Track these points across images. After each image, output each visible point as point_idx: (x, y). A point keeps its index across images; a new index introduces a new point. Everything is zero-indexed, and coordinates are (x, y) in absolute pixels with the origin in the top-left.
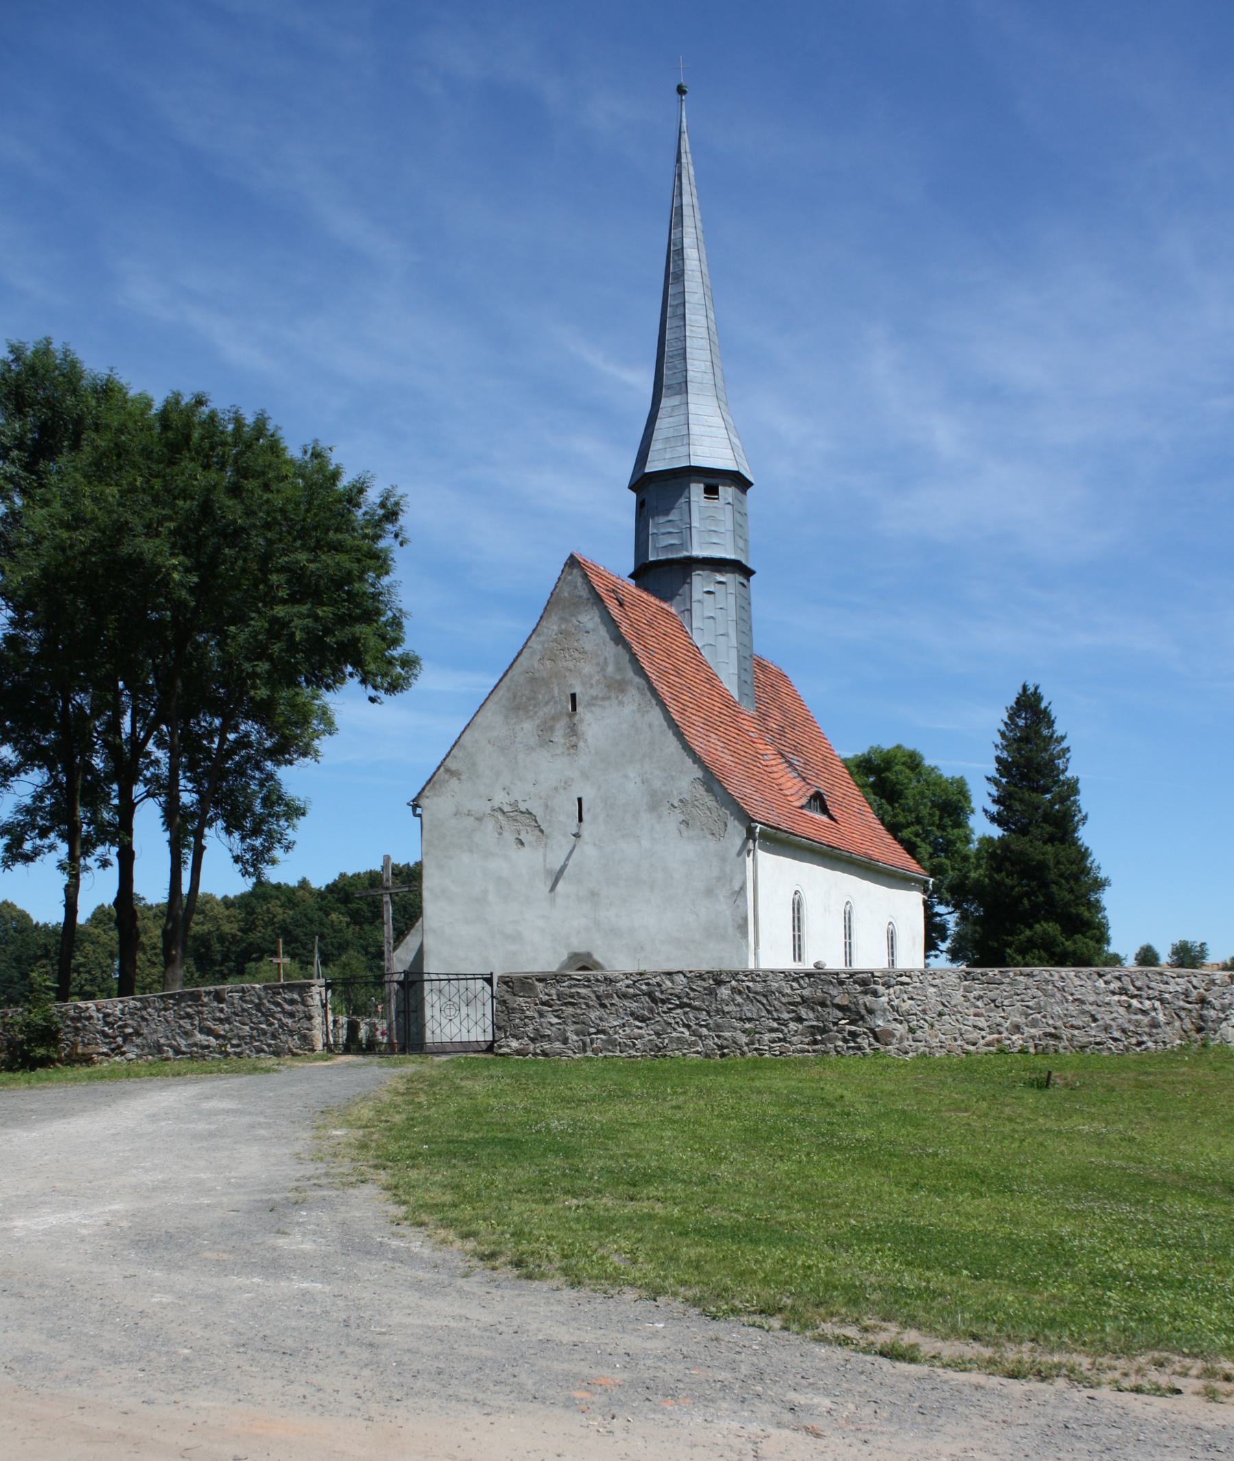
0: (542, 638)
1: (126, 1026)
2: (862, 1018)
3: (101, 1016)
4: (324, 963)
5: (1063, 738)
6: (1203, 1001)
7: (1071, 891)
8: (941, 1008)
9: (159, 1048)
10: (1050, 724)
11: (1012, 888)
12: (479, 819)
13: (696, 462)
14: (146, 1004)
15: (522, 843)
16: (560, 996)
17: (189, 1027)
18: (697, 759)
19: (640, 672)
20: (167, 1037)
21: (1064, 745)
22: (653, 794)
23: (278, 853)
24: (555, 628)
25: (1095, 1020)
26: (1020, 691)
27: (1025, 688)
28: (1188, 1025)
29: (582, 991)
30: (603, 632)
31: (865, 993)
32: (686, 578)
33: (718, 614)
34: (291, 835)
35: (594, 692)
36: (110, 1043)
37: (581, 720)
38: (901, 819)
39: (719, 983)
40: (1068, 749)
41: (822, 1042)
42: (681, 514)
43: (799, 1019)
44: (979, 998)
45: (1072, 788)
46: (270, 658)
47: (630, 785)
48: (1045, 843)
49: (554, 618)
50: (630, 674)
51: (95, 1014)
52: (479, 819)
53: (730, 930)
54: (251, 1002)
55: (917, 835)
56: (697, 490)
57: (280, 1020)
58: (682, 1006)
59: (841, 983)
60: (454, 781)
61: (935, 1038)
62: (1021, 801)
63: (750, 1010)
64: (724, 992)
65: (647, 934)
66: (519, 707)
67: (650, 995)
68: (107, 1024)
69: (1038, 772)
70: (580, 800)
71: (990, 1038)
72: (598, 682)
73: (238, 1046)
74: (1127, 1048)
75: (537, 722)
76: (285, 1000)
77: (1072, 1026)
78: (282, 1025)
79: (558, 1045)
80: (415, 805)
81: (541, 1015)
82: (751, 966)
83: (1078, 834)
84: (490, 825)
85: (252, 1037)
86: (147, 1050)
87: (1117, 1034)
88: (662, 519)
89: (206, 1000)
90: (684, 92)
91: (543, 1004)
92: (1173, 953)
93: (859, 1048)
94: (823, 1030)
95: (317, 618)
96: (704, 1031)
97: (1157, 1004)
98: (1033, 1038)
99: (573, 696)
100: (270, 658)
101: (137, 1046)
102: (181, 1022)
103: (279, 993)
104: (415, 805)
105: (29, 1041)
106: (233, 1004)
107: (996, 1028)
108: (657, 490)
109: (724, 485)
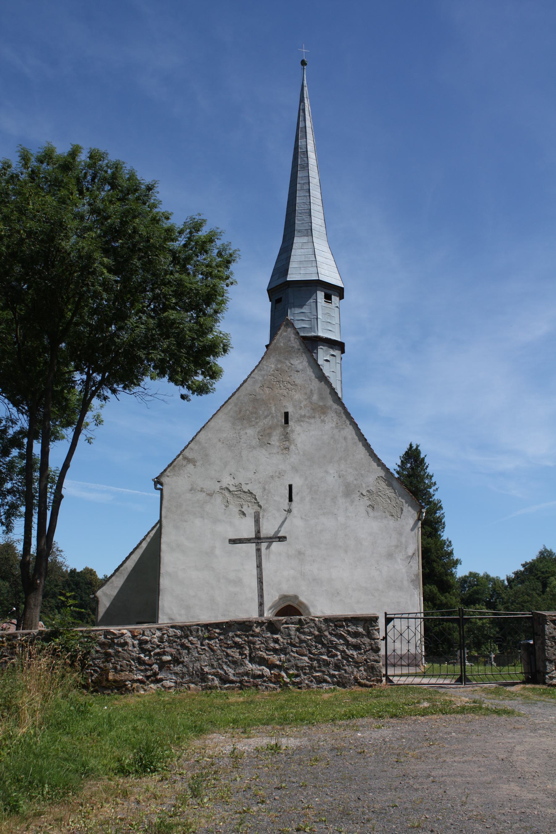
0: (263, 372)
1: (164, 653)
3: (136, 642)
4: (44, 597)
12: (210, 495)
15: (244, 514)
17: (237, 656)
20: (212, 666)
22: (347, 486)
24: (273, 366)
26: (408, 447)
27: (411, 446)
36: (146, 670)
37: (293, 431)
42: (311, 309)
47: (331, 478)
49: (272, 360)
50: (330, 402)
51: (129, 641)
53: (406, 583)
54: (311, 634)
56: (320, 295)
57: (344, 651)
60: (190, 467)
68: (143, 650)
70: (290, 487)
72: (305, 406)
73: (297, 676)
76: (349, 633)
78: (346, 657)
80: (158, 482)
85: (311, 667)
86: (187, 678)
88: (297, 311)
89: (257, 630)
90: (306, 64)
99: (286, 415)
101: (176, 674)
102: (229, 651)
103: (342, 626)
104: (158, 482)
106: (289, 635)
109: (334, 295)
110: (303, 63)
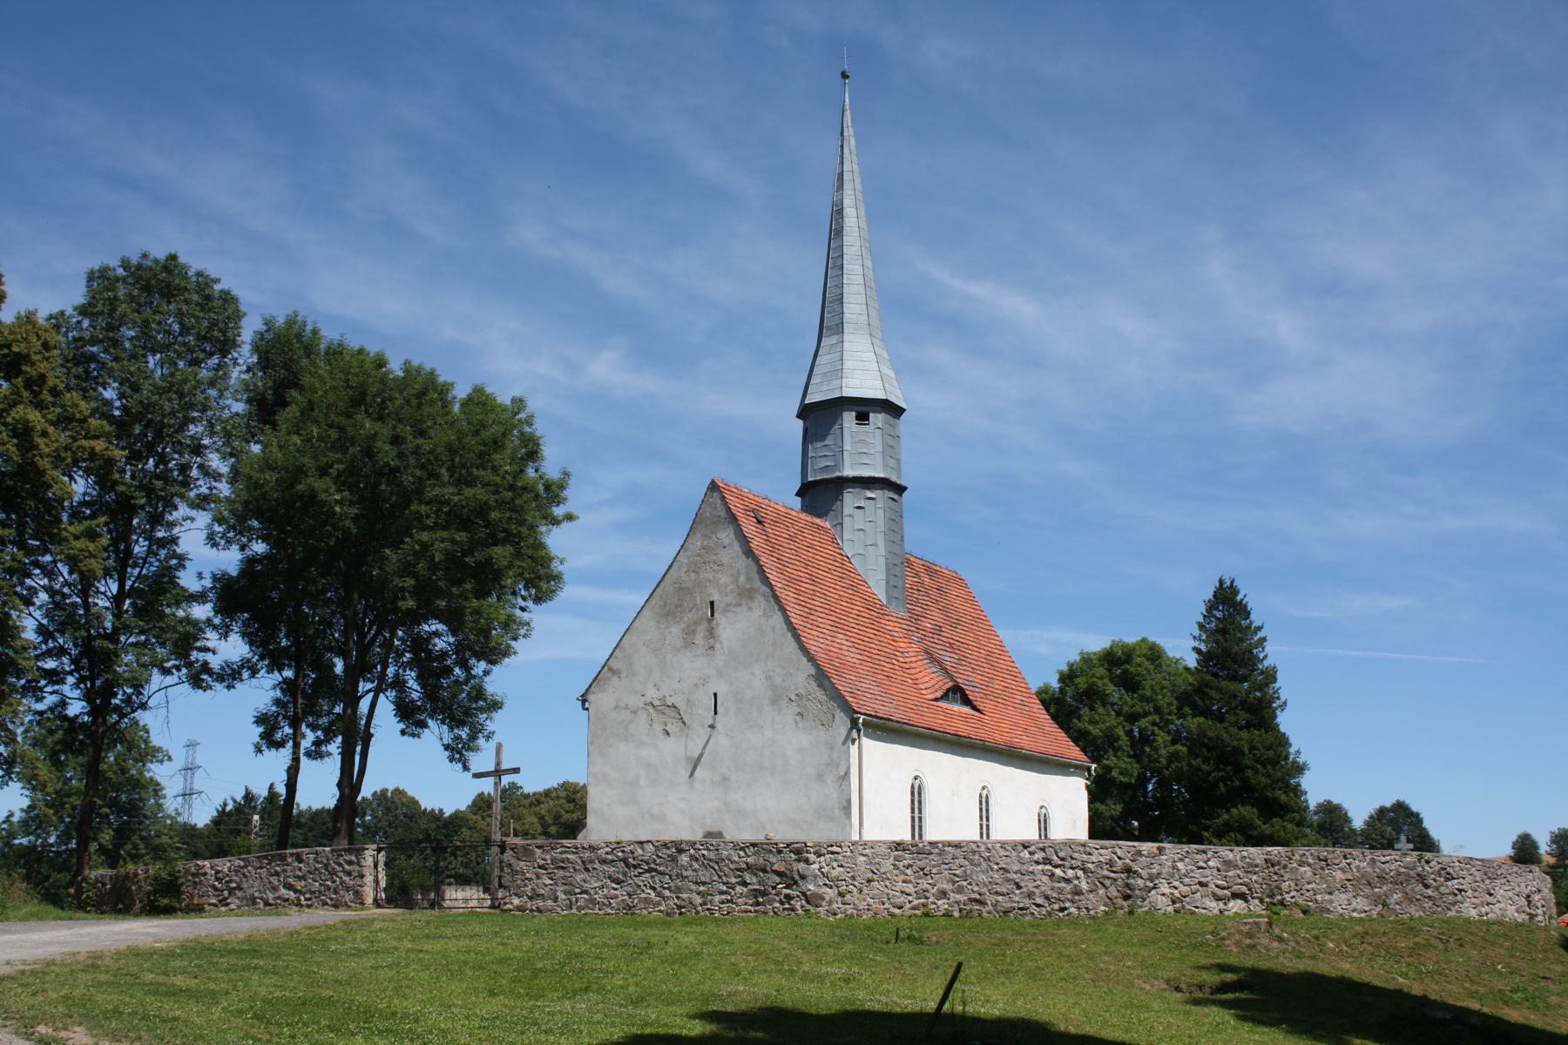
2: (796, 883)
5: (1259, 628)
6: (1128, 870)
7: (1268, 776)
8: (870, 875)
9: (253, 901)
10: (1247, 615)
11: (1209, 773)
12: (634, 712)
13: (847, 393)
14: (247, 863)
16: (553, 860)
18: (811, 659)
19: (766, 580)
21: (1260, 634)
22: (774, 688)
23: (481, 741)
25: (1019, 887)
27: (1221, 582)
28: (1113, 892)
29: (571, 857)
30: (737, 547)
31: (799, 861)
32: (838, 496)
33: (867, 527)
34: (490, 726)
35: (728, 600)
38: (1138, 709)
39: (680, 851)
40: (1264, 639)
41: (762, 904)
43: (745, 884)
44: (909, 866)
45: (1271, 676)
46: (415, 575)
48: (1241, 729)
50: (758, 584)
52: (634, 712)
55: (1154, 724)
56: (849, 418)
58: (650, 870)
59: (780, 852)
61: (864, 902)
62: (1218, 689)
63: (704, 875)
64: (684, 859)
65: (766, 811)
66: (668, 613)
67: (624, 860)
68: (217, 879)
69: (1234, 661)
71: (916, 902)
74: (1049, 914)
75: (683, 626)
77: (997, 893)
79: (550, 903)
81: (538, 877)
82: (855, 837)
83: (1278, 720)
84: (643, 717)
87: (1040, 901)
88: (819, 445)
91: (540, 867)
92: (1553, 842)
93: (793, 909)
94: (764, 894)
95: (454, 542)
96: (667, 893)
97: (1080, 873)
98: (958, 903)
99: (712, 603)
100: (415, 575)
105: (156, 892)
107: (923, 894)
108: (819, 417)
110: (844, 76)
